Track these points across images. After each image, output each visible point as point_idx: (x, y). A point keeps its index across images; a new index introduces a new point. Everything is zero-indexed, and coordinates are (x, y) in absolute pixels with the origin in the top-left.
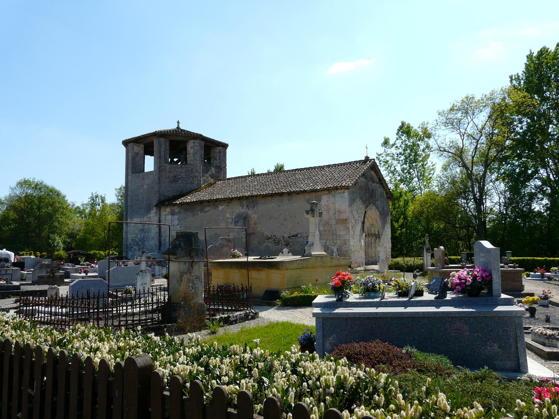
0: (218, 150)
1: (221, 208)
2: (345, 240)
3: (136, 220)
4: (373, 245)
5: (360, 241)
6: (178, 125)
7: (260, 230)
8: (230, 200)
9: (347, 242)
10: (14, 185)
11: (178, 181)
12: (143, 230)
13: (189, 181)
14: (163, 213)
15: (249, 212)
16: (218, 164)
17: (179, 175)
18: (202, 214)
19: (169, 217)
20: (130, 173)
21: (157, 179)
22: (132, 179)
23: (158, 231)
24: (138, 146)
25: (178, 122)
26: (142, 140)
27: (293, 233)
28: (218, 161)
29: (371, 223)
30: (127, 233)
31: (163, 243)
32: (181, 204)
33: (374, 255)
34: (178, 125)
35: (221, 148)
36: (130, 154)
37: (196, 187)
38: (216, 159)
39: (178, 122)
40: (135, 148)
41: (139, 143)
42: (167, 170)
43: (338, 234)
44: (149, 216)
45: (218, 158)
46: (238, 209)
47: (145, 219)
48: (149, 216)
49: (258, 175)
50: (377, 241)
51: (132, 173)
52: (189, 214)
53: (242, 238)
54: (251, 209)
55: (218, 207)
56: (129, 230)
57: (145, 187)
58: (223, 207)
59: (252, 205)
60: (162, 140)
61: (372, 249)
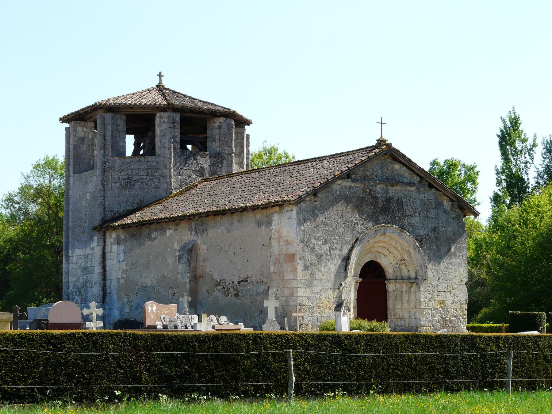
0: (217, 124)
1: (169, 233)
2: (292, 288)
3: (78, 252)
4: (405, 297)
5: (338, 287)
6: (160, 80)
7: (208, 271)
8: (175, 220)
9: (295, 292)
10: (28, 169)
11: (134, 185)
12: (85, 269)
13: (153, 185)
14: (109, 241)
15: (199, 241)
16: (218, 150)
17: (136, 174)
18: (149, 243)
19: (115, 247)
20: (71, 173)
21: (100, 184)
22: (74, 182)
23: (101, 270)
24: (84, 126)
25: (160, 75)
26: (89, 116)
27: (243, 276)
28: (218, 144)
29: (399, 257)
30: (68, 273)
31: (108, 291)
32: (124, 227)
33: (406, 315)
34: (160, 80)
35: (222, 120)
36: (71, 140)
37: (164, 194)
38: (214, 140)
39: (160, 75)
40: (79, 129)
41: (86, 121)
42: (117, 166)
43: (285, 278)
44: (92, 246)
45: (217, 137)
46: (184, 235)
47: (88, 251)
48: (92, 246)
49: (299, 163)
50: (413, 289)
51: (74, 173)
52: (135, 242)
53: (186, 283)
54: (199, 235)
55: (165, 231)
56: (70, 268)
57: (88, 196)
58: (171, 231)
59: (201, 228)
60: (108, 116)
61: (402, 303)
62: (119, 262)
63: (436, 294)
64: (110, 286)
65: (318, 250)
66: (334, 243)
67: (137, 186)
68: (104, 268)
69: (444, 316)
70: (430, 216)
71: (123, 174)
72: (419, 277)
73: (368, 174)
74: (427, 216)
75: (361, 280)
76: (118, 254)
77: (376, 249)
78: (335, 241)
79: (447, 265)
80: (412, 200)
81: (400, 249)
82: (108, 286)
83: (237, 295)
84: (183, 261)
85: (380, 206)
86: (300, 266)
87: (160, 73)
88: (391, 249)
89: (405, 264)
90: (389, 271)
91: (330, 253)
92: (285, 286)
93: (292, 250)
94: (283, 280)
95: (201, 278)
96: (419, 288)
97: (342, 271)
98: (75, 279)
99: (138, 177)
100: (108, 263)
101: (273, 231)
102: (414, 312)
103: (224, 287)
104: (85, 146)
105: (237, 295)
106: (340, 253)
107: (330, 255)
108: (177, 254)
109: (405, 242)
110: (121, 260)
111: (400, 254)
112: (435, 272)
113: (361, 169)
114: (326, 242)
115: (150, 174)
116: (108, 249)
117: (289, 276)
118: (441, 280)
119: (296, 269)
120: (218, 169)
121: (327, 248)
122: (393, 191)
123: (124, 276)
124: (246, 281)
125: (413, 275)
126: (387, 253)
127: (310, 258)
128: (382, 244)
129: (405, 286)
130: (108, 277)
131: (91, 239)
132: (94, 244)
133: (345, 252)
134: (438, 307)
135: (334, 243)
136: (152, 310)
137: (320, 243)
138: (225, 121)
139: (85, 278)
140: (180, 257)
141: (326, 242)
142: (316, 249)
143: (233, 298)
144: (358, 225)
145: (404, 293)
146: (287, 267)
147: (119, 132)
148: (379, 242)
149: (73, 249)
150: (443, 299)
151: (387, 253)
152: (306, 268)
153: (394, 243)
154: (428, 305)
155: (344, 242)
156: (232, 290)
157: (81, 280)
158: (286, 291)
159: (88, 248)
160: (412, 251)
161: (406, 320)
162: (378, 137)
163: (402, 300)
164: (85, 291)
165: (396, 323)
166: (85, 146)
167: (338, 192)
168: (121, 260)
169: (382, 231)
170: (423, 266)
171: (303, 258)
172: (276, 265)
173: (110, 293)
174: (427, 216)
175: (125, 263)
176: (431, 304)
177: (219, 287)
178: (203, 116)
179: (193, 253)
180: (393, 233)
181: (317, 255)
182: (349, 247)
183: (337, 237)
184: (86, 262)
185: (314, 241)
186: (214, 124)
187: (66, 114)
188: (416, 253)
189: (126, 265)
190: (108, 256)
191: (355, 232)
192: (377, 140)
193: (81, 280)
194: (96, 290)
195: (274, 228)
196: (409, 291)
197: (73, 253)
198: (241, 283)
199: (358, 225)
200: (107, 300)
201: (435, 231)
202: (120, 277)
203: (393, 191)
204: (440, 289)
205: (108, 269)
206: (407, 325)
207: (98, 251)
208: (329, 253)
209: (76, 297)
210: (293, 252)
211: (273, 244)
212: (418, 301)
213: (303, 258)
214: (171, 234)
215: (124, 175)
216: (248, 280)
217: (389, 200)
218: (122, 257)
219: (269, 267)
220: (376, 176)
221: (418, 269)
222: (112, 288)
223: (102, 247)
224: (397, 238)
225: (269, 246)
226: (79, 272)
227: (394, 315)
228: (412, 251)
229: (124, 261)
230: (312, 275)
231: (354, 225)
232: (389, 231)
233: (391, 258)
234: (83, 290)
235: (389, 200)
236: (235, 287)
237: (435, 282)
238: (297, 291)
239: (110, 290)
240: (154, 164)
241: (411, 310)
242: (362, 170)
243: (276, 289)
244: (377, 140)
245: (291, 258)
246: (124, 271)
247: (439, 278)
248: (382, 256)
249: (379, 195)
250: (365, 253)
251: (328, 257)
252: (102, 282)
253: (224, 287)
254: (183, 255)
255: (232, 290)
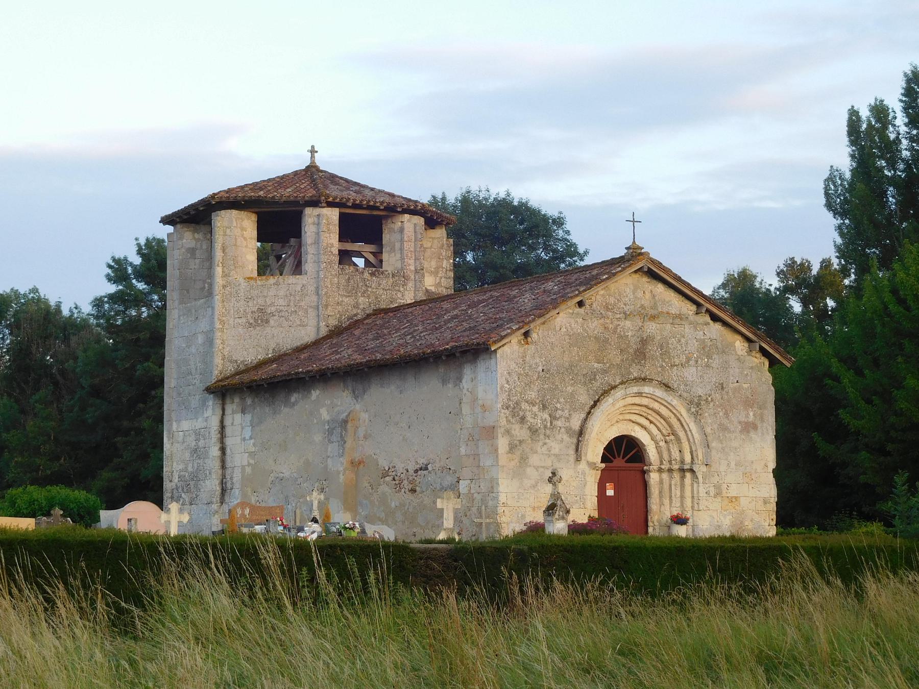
3: (186, 425)
6: (312, 157)
11: (267, 322)
12: (195, 451)
17: (272, 304)
27: (422, 461)
31: (229, 485)
39: (313, 151)
43: (482, 464)
47: (199, 424)
52: (267, 409)
62: (244, 439)
64: (231, 478)
65: (532, 421)
67: (272, 322)
68: (223, 450)
70: (713, 365)
71: (250, 304)
73: (612, 300)
74: (708, 366)
76: (243, 428)
78: (558, 406)
80: (683, 340)
82: (228, 477)
83: (413, 491)
84: (334, 438)
85: (631, 351)
86: (502, 443)
87: (313, 147)
92: (482, 476)
93: (489, 421)
94: (479, 466)
95: (361, 466)
98: (181, 467)
99: (273, 309)
100: (229, 442)
101: (465, 391)
103: (394, 479)
104: (197, 261)
105: (413, 491)
106: (567, 424)
107: (553, 427)
108: (327, 427)
110: (247, 438)
113: (602, 292)
114: (544, 407)
115: (292, 304)
116: (228, 421)
117: (487, 462)
119: (496, 450)
120: (399, 295)
121: (546, 416)
122: (652, 328)
123: (252, 462)
124: (426, 469)
127: (519, 432)
130: (229, 464)
131: (203, 404)
132: (209, 413)
133: (576, 424)
135: (557, 409)
136: (243, 515)
137: (535, 409)
138: (409, 221)
139: (195, 465)
140: (330, 432)
141: (544, 407)
142: (529, 418)
143: (409, 496)
146: (484, 447)
147: (245, 239)
149: (178, 421)
152: (512, 448)
156: (405, 482)
157: (190, 469)
158: (482, 485)
159: (200, 419)
162: (629, 243)
164: (196, 486)
166: (197, 261)
167: (564, 330)
168: (247, 438)
171: (508, 432)
172: (469, 443)
173: (232, 489)
174: (708, 366)
175: (252, 441)
177: (387, 479)
178: (375, 213)
179: (349, 425)
181: (530, 428)
182: (583, 416)
184: (197, 440)
185: (524, 406)
186: (392, 226)
187: (170, 212)
189: (254, 444)
190: (228, 431)
192: (627, 248)
193: (190, 469)
194: (212, 484)
195: (466, 387)
197: (178, 426)
198: (419, 472)
200: (227, 498)
201: (722, 388)
202: (245, 463)
203: (652, 328)
205: (228, 451)
207: (215, 423)
208: (549, 424)
209: (183, 495)
210: (492, 424)
211: (463, 412)
213: (508, 432)
214: (318, 396)
215: (252, 306)
216: (429, 466)
217: (644, 342)
218: (248, 433)
219: (459, 447)
220: (625, 304)
222: (235, 480)
223: (220, 417)
225: (459, 413)
226: (187, 455)
229: (251, 438)
230: (524, 459)
234: (192, 483)
235: (644, 342)
236: (411, 478)
238: (498, 484)
239: (232, 484)
240: (299, 288)
242: (603, 295)
243: (469, 481)
244: (627, 248)
245: (490, 432)
246: (252, 454)
249: (630, 334)
250: (609, 424)
251: (548, 432)
252: (220, 472)
253: (394, 479)
254: (334, 429)
255: (405, 482)
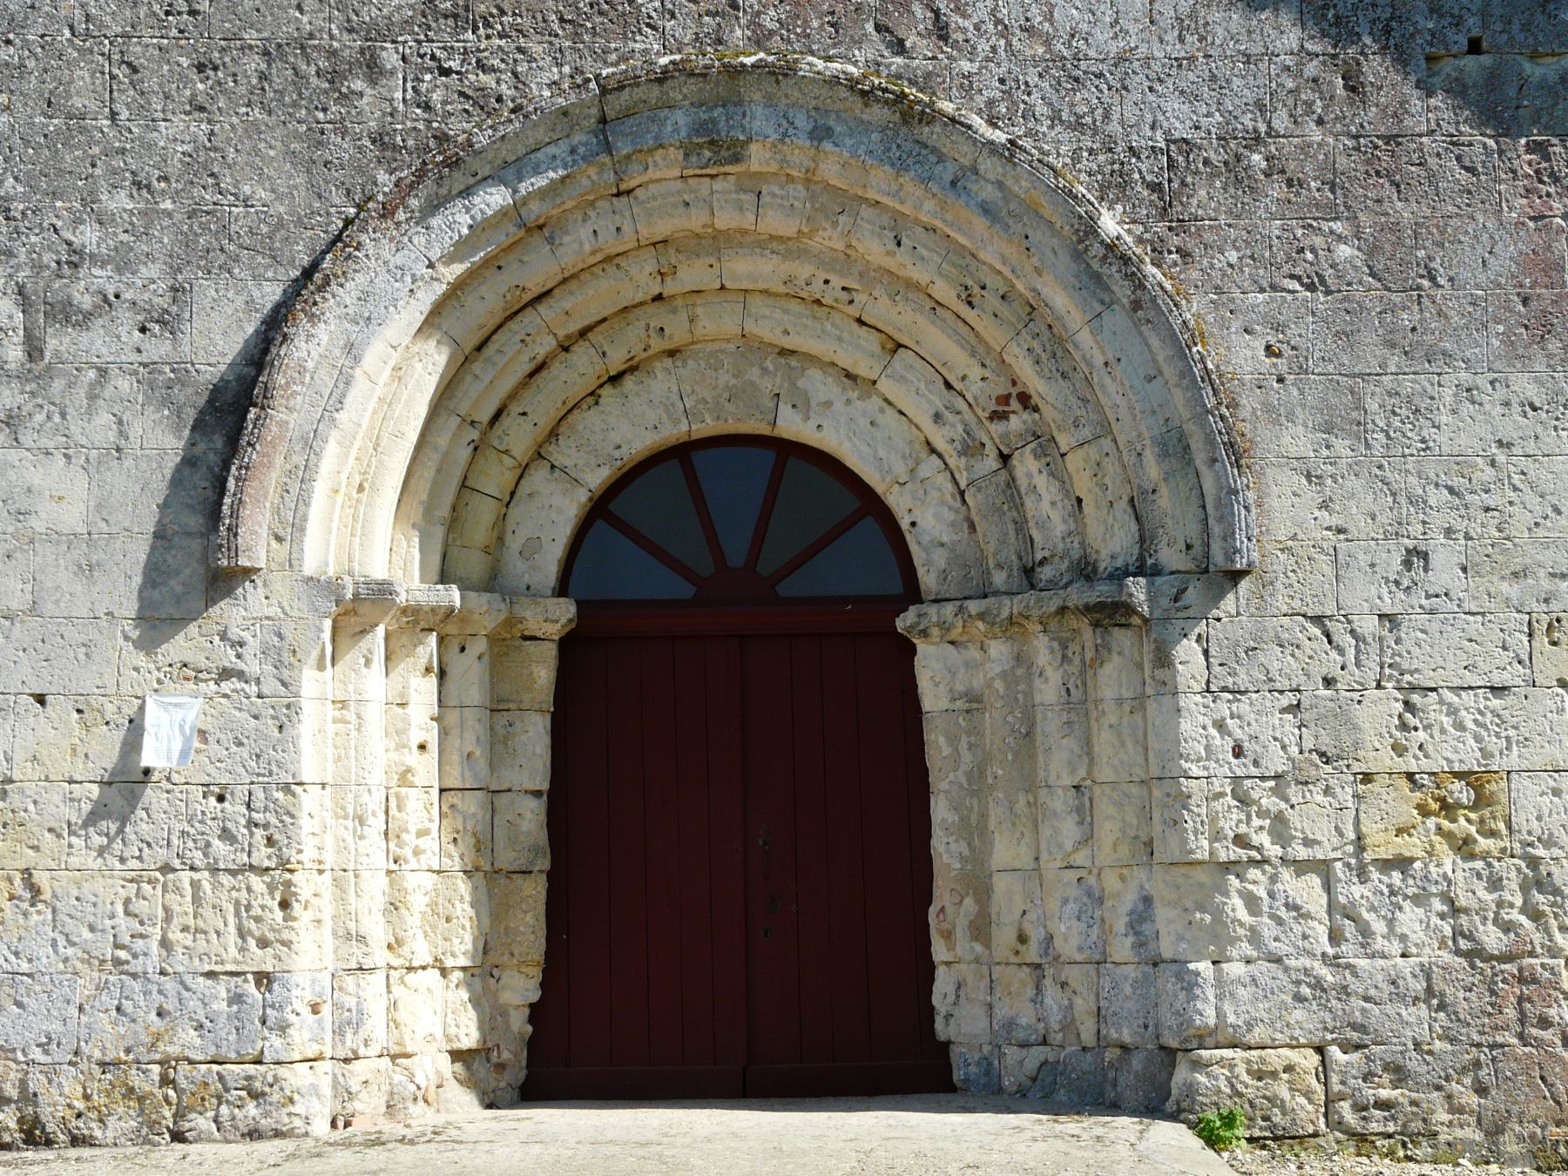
4: (1058, 765)
29: (979, 385)
33: (1070, 937)
50: (1112, 680)
63: (1378, 712)
66: (76, 259)
69: (1492, 939)
72: (1170, 556)
75: (903, 622)
77: (718, 322)
78: (89, 236)
79: (1513, 425)
81: (944, 291)
88: (882, 310)
89: (1043, 442)
90: (928, 520)
91: (34, 350)
96: (1163, 659)
97: (195, 521)
102: (1130, 899)
106: (158, 348)
109: (980, 224)
111: (977, 347)
112: (1360, 505)
118: (1445, 559)
125: (1112, 539)
126: (860, 355)
128: (744, 268)
129: (1042, 649)
133: (215, 340)
134: (1411, 846)
135: (76, 259)
144: (373, 69)
145: (1050, 725)
148: (717, 242)
150: (1470, 759)
151: (860, 355)
153: (874, 248)
154: (1280, 827)
155: (206, 246)
160: (1061, 300)
161: (1073, 974)
163: (1031, 784)
165: (1002, 1012)
169: (680, 119)
170: (1197, 443)
176: (1319, 820)
180: (820, 134)
182: (271, 293)
183: (120, 202)
188: (1117, 319)
191: (340, 149)
196: (1079, 705)
199: (373, 69)
204: (1433, 653)
206: (1088, 1037)
212: (1161, 788)
221: (1153, 470)
224: (880, 182)
227: (981, 929)
228: (1061, 300)
231: (334, 77)
232: (760, 119)
233: (920, 401)
237: (1365, 598)
241: (1111, 882)
247: (1417, 557)
248: (819, 385)
